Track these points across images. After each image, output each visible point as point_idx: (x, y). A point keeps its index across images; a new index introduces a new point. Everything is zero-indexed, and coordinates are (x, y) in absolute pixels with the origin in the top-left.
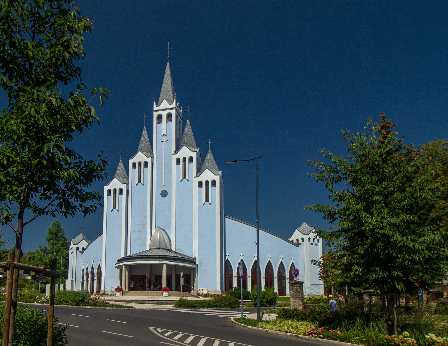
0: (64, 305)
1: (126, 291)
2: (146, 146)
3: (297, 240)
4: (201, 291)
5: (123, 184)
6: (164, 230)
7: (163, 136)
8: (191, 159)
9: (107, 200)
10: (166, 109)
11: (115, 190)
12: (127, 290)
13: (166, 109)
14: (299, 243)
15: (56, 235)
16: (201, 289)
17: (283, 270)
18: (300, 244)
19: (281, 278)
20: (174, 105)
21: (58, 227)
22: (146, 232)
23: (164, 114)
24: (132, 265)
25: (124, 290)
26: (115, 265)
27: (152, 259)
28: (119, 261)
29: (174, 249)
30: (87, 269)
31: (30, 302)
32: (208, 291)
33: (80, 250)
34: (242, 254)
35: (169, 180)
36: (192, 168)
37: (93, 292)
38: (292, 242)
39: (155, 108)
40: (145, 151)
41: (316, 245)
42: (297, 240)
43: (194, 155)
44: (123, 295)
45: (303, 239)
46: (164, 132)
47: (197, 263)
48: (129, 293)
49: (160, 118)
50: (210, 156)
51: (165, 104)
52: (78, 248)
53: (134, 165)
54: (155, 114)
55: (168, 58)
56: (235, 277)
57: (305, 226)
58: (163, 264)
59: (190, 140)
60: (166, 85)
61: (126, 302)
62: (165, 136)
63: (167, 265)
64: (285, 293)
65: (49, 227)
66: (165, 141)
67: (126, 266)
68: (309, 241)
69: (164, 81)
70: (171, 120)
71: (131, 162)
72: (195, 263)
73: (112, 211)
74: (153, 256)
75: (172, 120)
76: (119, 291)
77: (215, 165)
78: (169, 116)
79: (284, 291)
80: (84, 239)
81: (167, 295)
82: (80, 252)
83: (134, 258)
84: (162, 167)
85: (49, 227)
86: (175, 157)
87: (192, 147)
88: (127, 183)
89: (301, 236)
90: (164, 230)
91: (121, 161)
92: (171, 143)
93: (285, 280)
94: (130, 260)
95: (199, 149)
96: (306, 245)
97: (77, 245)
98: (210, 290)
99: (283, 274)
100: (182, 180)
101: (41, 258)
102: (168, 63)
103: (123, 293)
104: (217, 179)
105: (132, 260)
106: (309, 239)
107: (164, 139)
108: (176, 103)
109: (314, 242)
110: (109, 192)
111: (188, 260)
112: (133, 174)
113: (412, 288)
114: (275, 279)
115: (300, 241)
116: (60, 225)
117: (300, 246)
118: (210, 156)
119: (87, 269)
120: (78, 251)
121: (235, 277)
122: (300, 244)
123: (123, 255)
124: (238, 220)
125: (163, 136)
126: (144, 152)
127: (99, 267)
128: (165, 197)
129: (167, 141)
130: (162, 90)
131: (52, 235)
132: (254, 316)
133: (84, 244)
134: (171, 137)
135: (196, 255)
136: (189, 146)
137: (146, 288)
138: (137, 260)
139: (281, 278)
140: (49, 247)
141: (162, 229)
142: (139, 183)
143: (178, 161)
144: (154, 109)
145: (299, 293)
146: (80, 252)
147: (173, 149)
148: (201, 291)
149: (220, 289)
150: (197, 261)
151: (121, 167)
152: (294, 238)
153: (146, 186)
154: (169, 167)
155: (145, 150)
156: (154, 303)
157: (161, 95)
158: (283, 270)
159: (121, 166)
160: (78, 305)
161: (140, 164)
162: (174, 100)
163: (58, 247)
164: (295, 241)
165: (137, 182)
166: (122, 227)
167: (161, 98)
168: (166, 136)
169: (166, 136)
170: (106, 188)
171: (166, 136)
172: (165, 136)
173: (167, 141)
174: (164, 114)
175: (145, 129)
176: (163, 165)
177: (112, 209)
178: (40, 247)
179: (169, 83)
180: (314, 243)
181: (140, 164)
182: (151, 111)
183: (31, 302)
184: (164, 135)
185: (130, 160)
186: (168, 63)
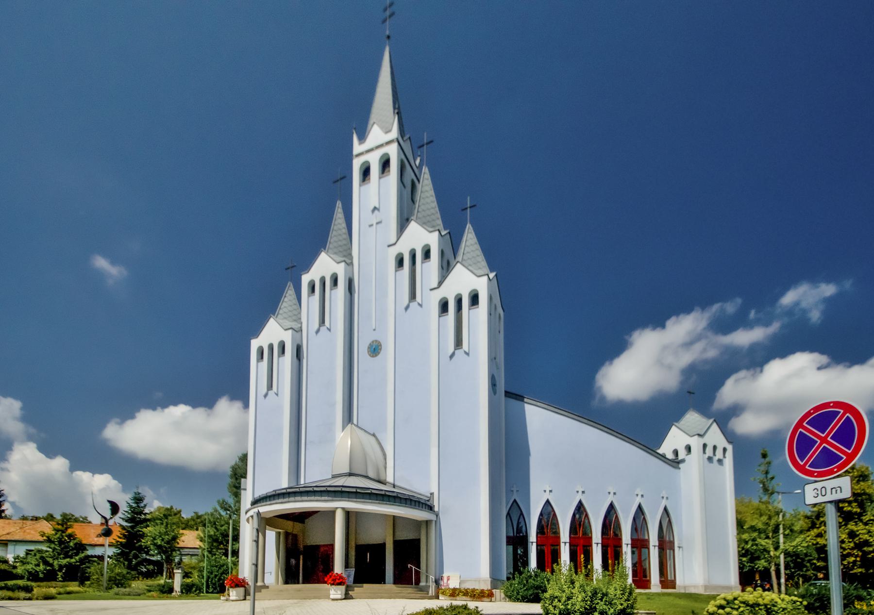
2: (340, 243)
3: (676, 452)
6: (374, 435)
9: (257, 371)
11: (271, 347)
14: (680, 457)
17: (644, 523)
18: (683, 461)
20: (394, 133)
29: (390, 479)
36: (430, 270)
38: (663, 457)
39: (357, 148)
40: (335, 253)
41: (720, 461)
42: (676, 452)
45: (689, 449)
47: (436, 509)
50: (469, 239)
59: (428, 218)
62: (376, 212)
64: (649, 581)
66: (377, 223)
68: (704, 452)
71: (306, 279)
72: (431, 508)
77: (480, 260)
78: (385, 164)
79: (645, 576)
86: (393, 252)
89: (685, 440)
90: (374, 435)
96: (693, 463)
99: (644, 535)
104: (482, 285)
106: (705, 446)
109: (714, 454)
111: (394, 497)
112: (310, 304)
113: (146, 550)
115: (682, 455)
118: (469, 239)
121: (627, 544)
122: (683, 461)
124: (539, 404)
126: (332, 256)
135: (435, 490)
136: (424, 223)
139: (640, 544)
141: (369, 434)
144: (355, 152)
149: (488, 576)
150: (436, 504)
152: (666, 449)
158: (644, 523)
159: (290, 293)
161: (323, 281)
162: (395, 118)
164: (670, 456)
165: (316, 326)
170: (255, 344)
171: (378, 210)
175: (340, 205)
180: (716, 458)
182: (348, 156)
184: (375, 208)
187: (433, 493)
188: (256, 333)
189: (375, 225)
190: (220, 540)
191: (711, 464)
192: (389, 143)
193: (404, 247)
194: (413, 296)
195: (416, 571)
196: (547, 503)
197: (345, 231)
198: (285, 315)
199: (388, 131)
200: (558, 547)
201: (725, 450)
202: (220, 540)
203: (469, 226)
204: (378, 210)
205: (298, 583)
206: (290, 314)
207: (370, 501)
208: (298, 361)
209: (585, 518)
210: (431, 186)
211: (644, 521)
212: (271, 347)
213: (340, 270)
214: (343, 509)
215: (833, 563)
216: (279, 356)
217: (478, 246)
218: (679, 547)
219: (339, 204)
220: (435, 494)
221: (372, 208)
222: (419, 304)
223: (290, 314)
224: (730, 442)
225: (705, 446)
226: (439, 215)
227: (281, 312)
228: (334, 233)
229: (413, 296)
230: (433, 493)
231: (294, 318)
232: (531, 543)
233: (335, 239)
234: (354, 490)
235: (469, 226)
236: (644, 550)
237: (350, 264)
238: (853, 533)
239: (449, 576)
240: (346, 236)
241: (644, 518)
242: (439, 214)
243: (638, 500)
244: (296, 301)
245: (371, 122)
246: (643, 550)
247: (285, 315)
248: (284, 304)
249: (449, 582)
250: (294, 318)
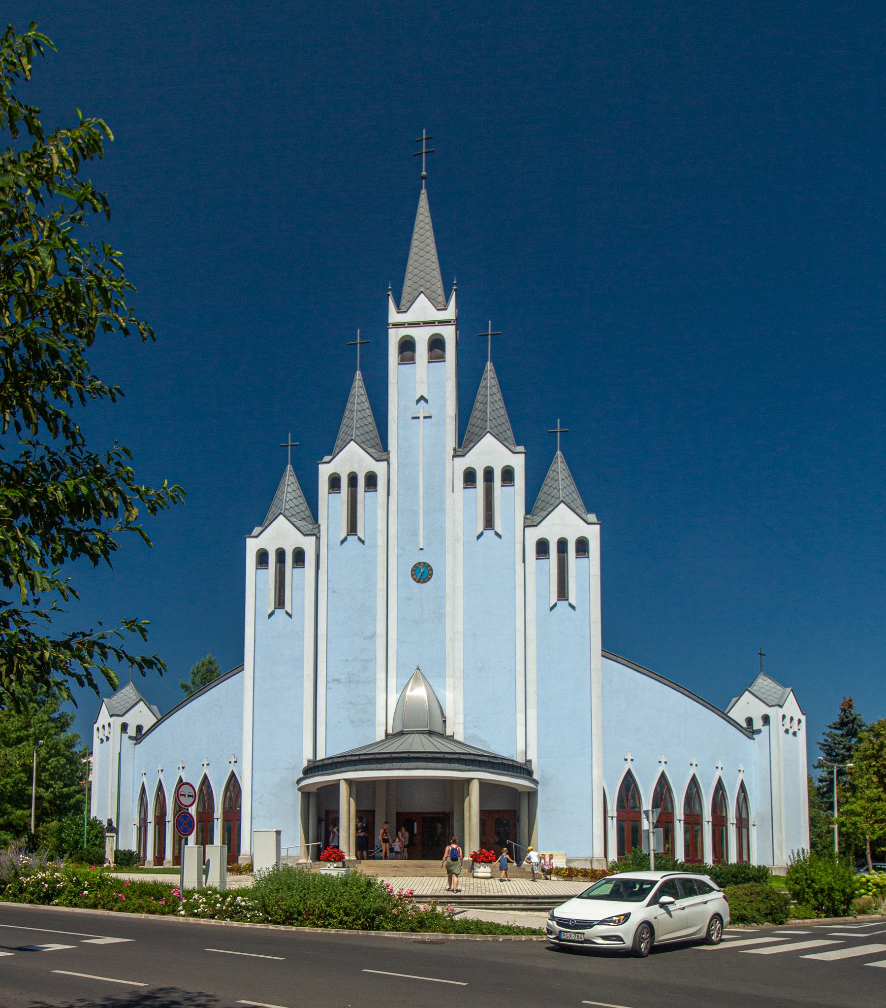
0: (316, 926)
3: (749, 721)
4: (547, 859)
5: (305, 535)
7: (418, 401)
8: (508, 475)
12: (353, 858)
16: (547, 853)
18: (759, 732)
19: (693, 821)
20: (450, 313)
22: (373, 681)
23: (421, 336)
27: (440, 765)
30: (160, 787)
31: (150, 912)
32: (568, 861)
33: (132, 731)
34: (629, 754)
35: (437, 533)
37: (164, 858)
39: (394, 317)
41: (795, 734)
42: (749, 721)
43: (518, 462)
45: (766, 719)
46: (422, 391)
47: (535, 776)
49: (407, 347)
50: (559, 468)
52: (124, 727)
53: (335, 482)
54: (394, 337)
55: (424, 178)
56: (612, 818)
57: (763, 683)
58: (469, 781)
60: (422, 253)
62: (422, 402)
63: (483, 784)
66: (425, 417)
67: (349, 782)
69: (414, 243)
70: (441, 358)
71: (325, 471)
73: (270, 616)
74: (406, 755)
78: (436, 345)
80: (141, 700)
81: (489, 875)
82: (130, 738)
83: (377, 759)
86: (462, 464)
88: (316, 531)
91: (289, 467)
97: (122, 716)
98: (572, 855)
99: (722, 811)
100: (481, 534)
102: (424, 191)
105: (371, 766)
106: (784, 717)
107: (422, 410)
110: (262, 558)
114: (677, 823)
115: (758, 724)
117: (755, 736)
118: (559, 468)
119: (160, 787)
120: (125, 736)
121: (612, 818)
122: (759, 732)
125: (418, 401)
127: (233, 786)
128: (424, 582)
129: (430, 417)
130: (410, 268)
132: (439, 909)
133: (142, 715)
138: (387, 765)
139: (693, 821)
144: (391, 321)
146: (130, 738)
147: (451, 441)
148: (547, 859)
151: (292, 486)
152: (739, 713)
153: (375, 546)
156: (519, 906)
157: (407, 283)
159: (290, 485)
160: (371, 928)
162: (447, 299)
166: (305, 665)
167: (406, 290)
168: (426, 401)
170: (252, 546)
171: (426, 401)
172: (422, 402)
173: (430, 417)
174: (421, 336)
176: (417, 488)
177: (272, 608)
179: (428, 249)
182: (384, 325)
183: (153, 913)
184: (422, 398)
185: (322, 467)
186: (424, 191)
187: (531, 760)
189: (421, 418)
191: (787, 735)
195: (515, 846)
196: (629, 776)
200: (639, 823)
201: (799, 721)
207: (505, 772)
209: (666, 792)
211: (697, 795)
214: (479, 779)
215: (707, 844)
220: (533, 761)
221: (418, 397)
224: (803, 714)
225: (784, 717)
230: (531, 760)
232: (610, 818)
234: (487, 759)
236: (201, 810)
239: (552, 855)
241: (723, 794)
243: (718, 773)
249: (552, 861)
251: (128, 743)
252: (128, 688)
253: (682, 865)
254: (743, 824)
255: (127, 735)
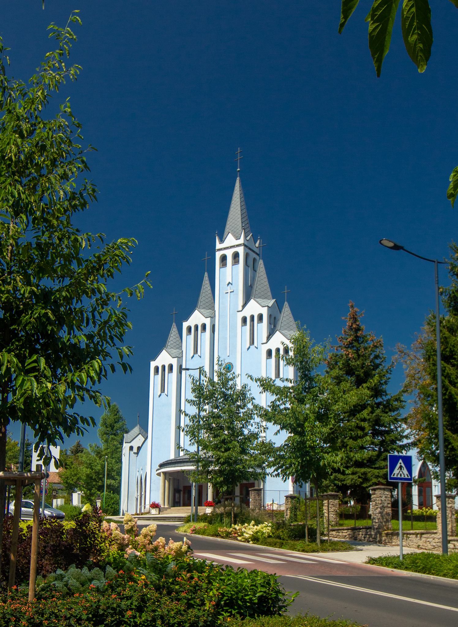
1: (164, 508)
2: (207, 301)
7: (228, 285)
9: (154, 381)
10: (231, 247)
11: (164, 367)
12: (166, 506)
13: (231, 247)
15: (112, 427)
21: (116, 415)
23: (229, 254)
24: (171, 473)
25: (162, 506)
26: (157, 470)
28: (162, 466)
30: (141, 479)
33: (135, 450)
36: (262, 329)
39: (218, 246)
40: (204, 308)
44: (160, 513)
48: (169, 510)
49: (224, 258)
50: (286, 309)
51: (230, 240)
52: (131, 448)
54: (218, 255)
55: (239, 171)
61: (143, 520)
62: (230, 285)
65: (102, 417)
66: (231, 292)
67: (163, 472)
71: (185, 325)
75: (239, 262)
76: (154, 508)
78: (236, 256)
80: (140, 434)
82: (134, 453)
84: (226, 330)
85: (102, 417)
86: (240, 316)
87: (265, 298)
92: (237, 294)
93: (431, 487)
94: (170, 466)
95: (275, 300)
101: (90, 464)
103: (160, 511)
105: (168, 466)
108: (246, 237)
112: (188, 341)
116: (118, 412)
119: (141, 479)
120: (132, 452)
123: (172, 457)
129: (233, 292)
131: (107, 427)
134: (238, 285)
137: (203, 504)
138: (176, 465)
140: (103, 446)
142: (195, 355)
143: (244, 320)
145: (256, 500)
146: (134, 453)
154: (233, 328)
155: (204, 306)
159: (174, 330)
161: (196, 327)
163: (114, 445)
169: (232, 284)
170: (153, 364)
173: (233, 292)
176: (227, 327)
178: (91, 447)
179: (238, 207)
181: (196, 327)
182: (213, 250)
184: (229, 283)
185: (184, 323)
186: (238, 178)
188: (154, 358)
189: (229, 293)
190: (93, 478)
192: (238, 246)
193: (248, 312)
194: (252, 342)
197: (210, 292)
198: (172, 346)
199: (238, 238)
202: (93, 478)
203: (286, 303)
204: (232, 284)
205: (180, 506)
206: (175, 344)
208: (180, 375)
210: (264, 271)
212: (164, 367)
213: (208, 322)
216: (169, 373)
217: (291, 315)
218: (435, 486)
219: (206, 275)
221: (227, 283)
222: (255, 347)
223: (175, 344)
226: (269, 290)
227: (169, 344)
228: (204, 295)
229: (252, 342)
231: (177, 346)
233: (204, 299)
235: (286, 303)
237: (213, 317)
238: (101, 490)
240: (211, 295)
242: (269, 289)
244: (179, 339)
245: (227, 230)
246: (427, 489)
247: (172, 346)
248: (171, 339)
250: (177, 346)
251: (133, 456)
252: (137, 427)
253: (210, 502)
254: (137, 499)
255: (133, 452)
